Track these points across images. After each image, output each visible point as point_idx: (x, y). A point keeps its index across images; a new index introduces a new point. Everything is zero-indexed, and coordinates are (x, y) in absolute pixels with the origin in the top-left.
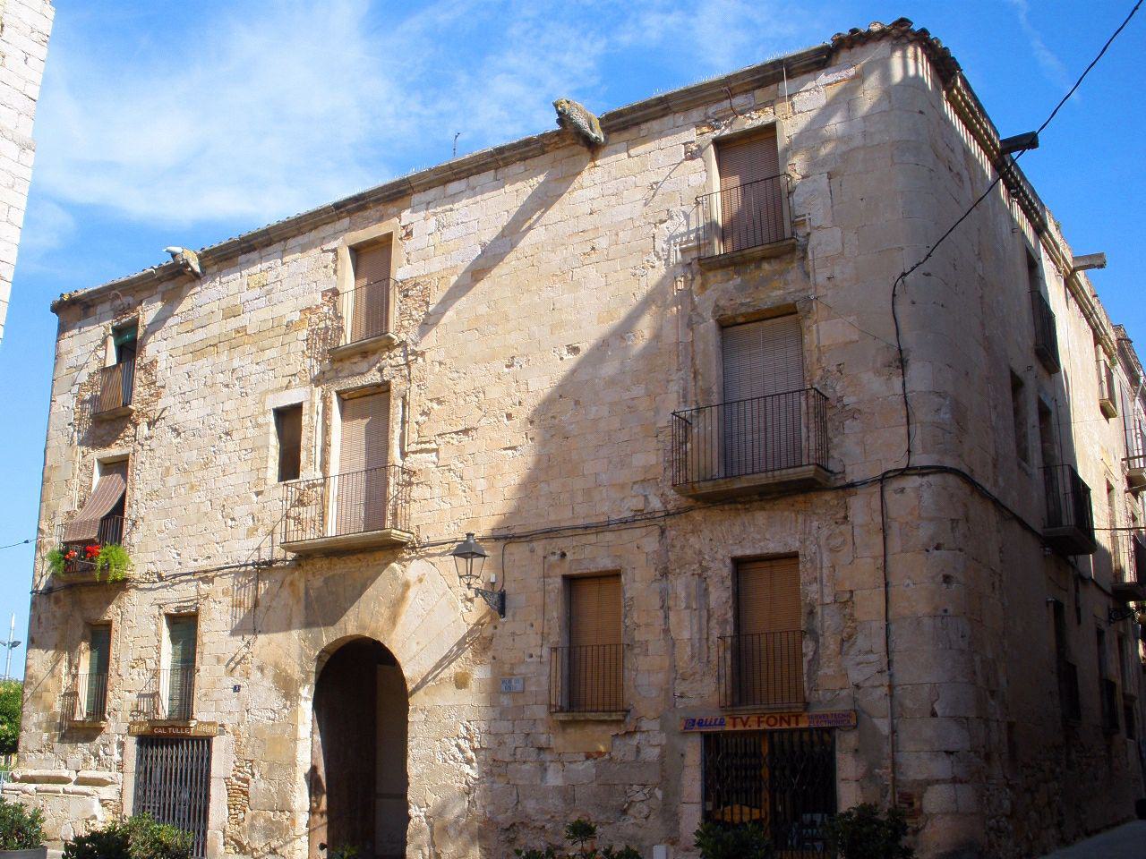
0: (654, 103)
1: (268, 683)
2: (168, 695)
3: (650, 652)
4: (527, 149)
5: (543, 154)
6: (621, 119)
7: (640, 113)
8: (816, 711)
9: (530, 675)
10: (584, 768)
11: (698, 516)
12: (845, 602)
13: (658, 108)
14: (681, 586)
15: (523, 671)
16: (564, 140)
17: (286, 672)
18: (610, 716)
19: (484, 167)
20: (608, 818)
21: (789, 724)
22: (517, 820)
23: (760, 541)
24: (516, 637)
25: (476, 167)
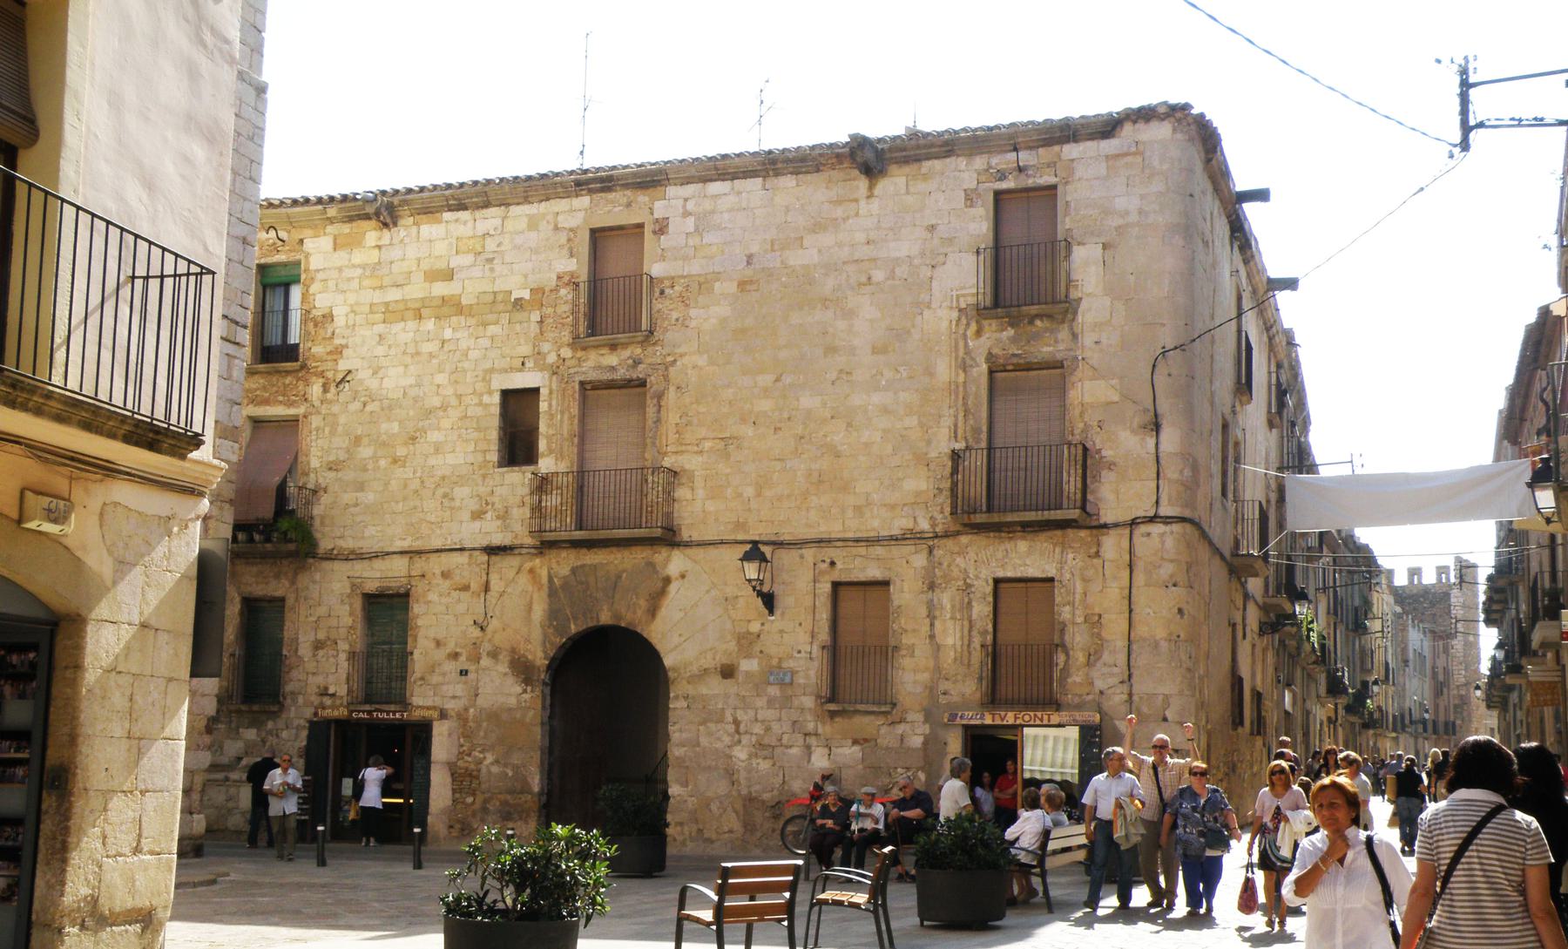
1: (503, 667)
11: (964, 539)
14: (946, 599)
22: (784, 798)
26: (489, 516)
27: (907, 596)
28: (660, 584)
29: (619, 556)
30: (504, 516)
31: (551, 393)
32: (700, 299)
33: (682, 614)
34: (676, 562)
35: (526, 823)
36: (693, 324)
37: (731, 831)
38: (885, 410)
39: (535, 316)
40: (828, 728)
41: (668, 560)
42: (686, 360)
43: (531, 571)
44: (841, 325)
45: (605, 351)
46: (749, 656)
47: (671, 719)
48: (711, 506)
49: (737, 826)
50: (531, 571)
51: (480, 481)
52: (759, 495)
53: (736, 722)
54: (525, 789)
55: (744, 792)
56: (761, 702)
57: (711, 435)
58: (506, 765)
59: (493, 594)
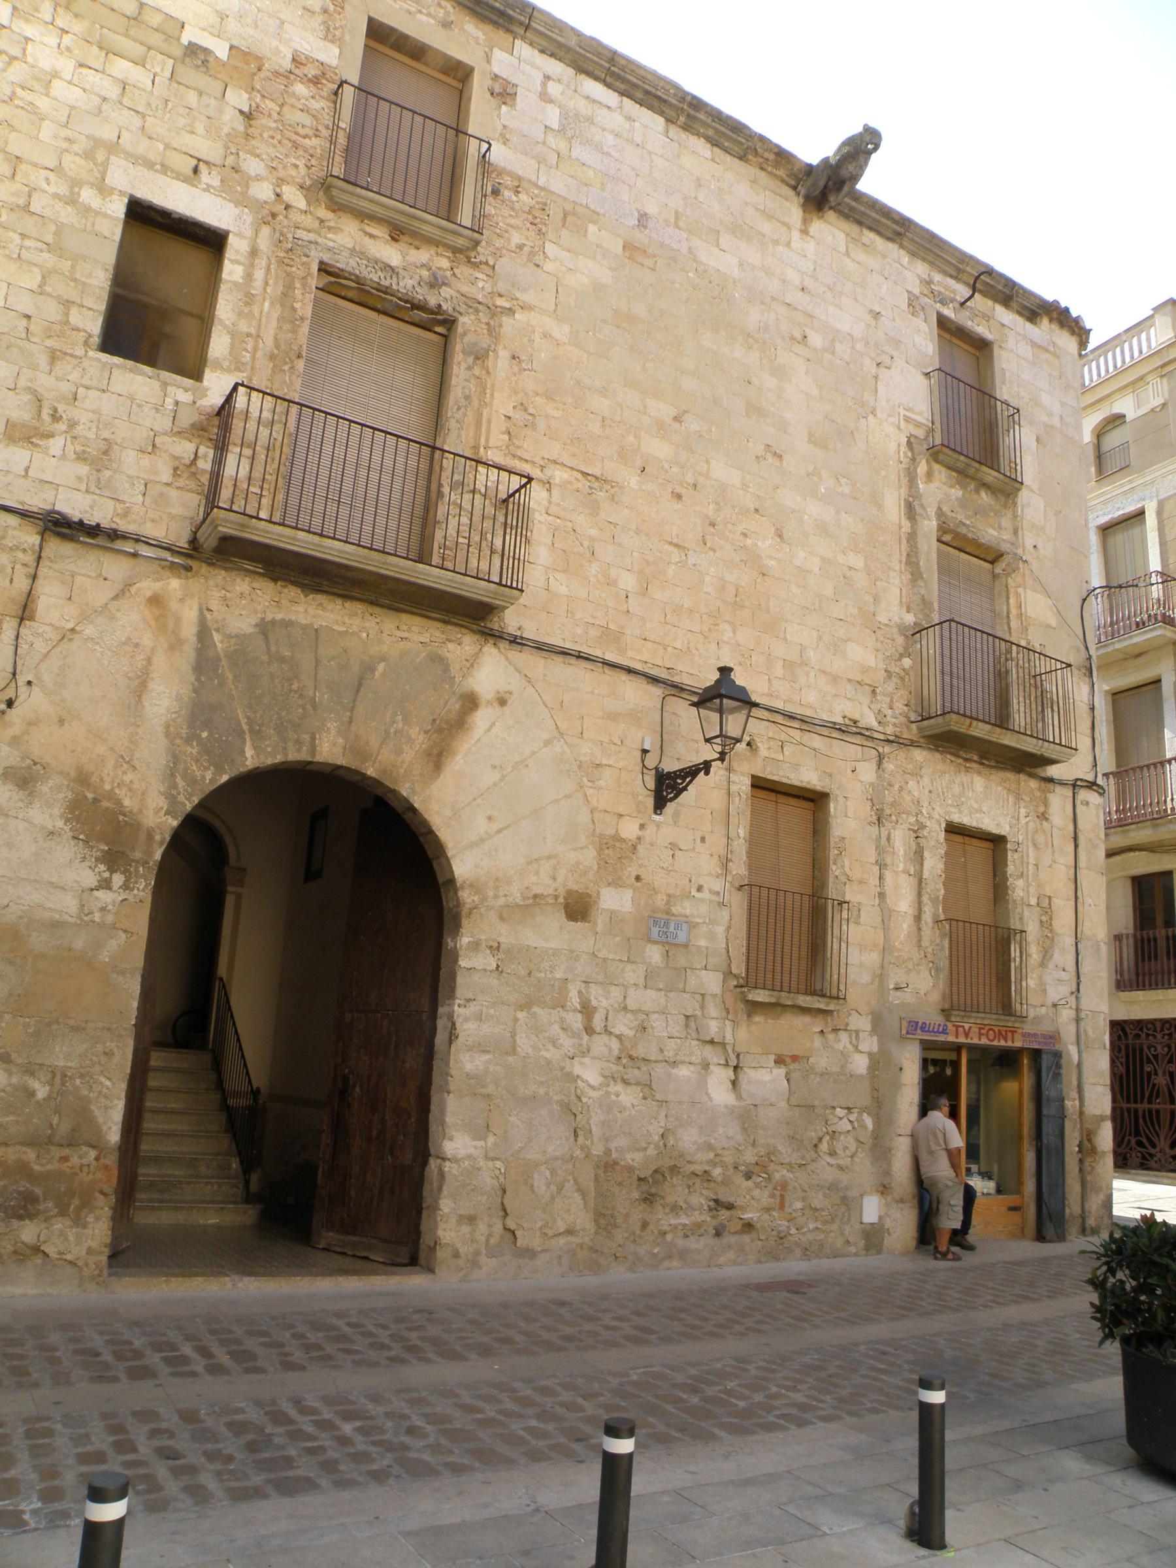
0: (897, 218)
1: (47, 814)
3: (862, 921)
4: (730, 133)
5: (740, 158)
6: (854, 203)
7: (874, 215)
8: (1029, 1028)
9: (698, 920)
10: (766, 1079)
11: (919, 755)
12: (1046, 908)
13: (896, 227)
14: (900, 839)
15: (688, 912)
16: (777, 165)
17: (119, 802)
18: (828, 1004)
19: (656, 103)
20: (803, 1158)
21: (1006, 1040)
22: (667, 1162)
23: (977, 811)
24: (678, 853)
25: (647, 93)
26: (56, 445)
27: (852, 823)
28: (455, 706)
29: (371, 624)
30: (99, 458)
31: (254, 253)
32: (565, 233)
33: (496, 776)
34: (491, 671)
35: (78, 1222)
36: (549, 266)
37: (570, 1232)
38: (823, 529)
39: (238, 99)
40: (742, 1033)
41: (472, 663)
42: (533, 318)
43: (156, 601)
44: (770, 382)
45: (381, 232)
46: (616, 883)
47: (461, 991)
48: (561, 585)
49: (583, 1220)
50: (156, 601)
51: (43, 361)
52: (644, 591)
53: (587, 1010)
54: (82, 1132)
55: (597, 1150)
56: (633, 974)
57: (572, 462)
58: (30, 1070)
59: (38, 635)
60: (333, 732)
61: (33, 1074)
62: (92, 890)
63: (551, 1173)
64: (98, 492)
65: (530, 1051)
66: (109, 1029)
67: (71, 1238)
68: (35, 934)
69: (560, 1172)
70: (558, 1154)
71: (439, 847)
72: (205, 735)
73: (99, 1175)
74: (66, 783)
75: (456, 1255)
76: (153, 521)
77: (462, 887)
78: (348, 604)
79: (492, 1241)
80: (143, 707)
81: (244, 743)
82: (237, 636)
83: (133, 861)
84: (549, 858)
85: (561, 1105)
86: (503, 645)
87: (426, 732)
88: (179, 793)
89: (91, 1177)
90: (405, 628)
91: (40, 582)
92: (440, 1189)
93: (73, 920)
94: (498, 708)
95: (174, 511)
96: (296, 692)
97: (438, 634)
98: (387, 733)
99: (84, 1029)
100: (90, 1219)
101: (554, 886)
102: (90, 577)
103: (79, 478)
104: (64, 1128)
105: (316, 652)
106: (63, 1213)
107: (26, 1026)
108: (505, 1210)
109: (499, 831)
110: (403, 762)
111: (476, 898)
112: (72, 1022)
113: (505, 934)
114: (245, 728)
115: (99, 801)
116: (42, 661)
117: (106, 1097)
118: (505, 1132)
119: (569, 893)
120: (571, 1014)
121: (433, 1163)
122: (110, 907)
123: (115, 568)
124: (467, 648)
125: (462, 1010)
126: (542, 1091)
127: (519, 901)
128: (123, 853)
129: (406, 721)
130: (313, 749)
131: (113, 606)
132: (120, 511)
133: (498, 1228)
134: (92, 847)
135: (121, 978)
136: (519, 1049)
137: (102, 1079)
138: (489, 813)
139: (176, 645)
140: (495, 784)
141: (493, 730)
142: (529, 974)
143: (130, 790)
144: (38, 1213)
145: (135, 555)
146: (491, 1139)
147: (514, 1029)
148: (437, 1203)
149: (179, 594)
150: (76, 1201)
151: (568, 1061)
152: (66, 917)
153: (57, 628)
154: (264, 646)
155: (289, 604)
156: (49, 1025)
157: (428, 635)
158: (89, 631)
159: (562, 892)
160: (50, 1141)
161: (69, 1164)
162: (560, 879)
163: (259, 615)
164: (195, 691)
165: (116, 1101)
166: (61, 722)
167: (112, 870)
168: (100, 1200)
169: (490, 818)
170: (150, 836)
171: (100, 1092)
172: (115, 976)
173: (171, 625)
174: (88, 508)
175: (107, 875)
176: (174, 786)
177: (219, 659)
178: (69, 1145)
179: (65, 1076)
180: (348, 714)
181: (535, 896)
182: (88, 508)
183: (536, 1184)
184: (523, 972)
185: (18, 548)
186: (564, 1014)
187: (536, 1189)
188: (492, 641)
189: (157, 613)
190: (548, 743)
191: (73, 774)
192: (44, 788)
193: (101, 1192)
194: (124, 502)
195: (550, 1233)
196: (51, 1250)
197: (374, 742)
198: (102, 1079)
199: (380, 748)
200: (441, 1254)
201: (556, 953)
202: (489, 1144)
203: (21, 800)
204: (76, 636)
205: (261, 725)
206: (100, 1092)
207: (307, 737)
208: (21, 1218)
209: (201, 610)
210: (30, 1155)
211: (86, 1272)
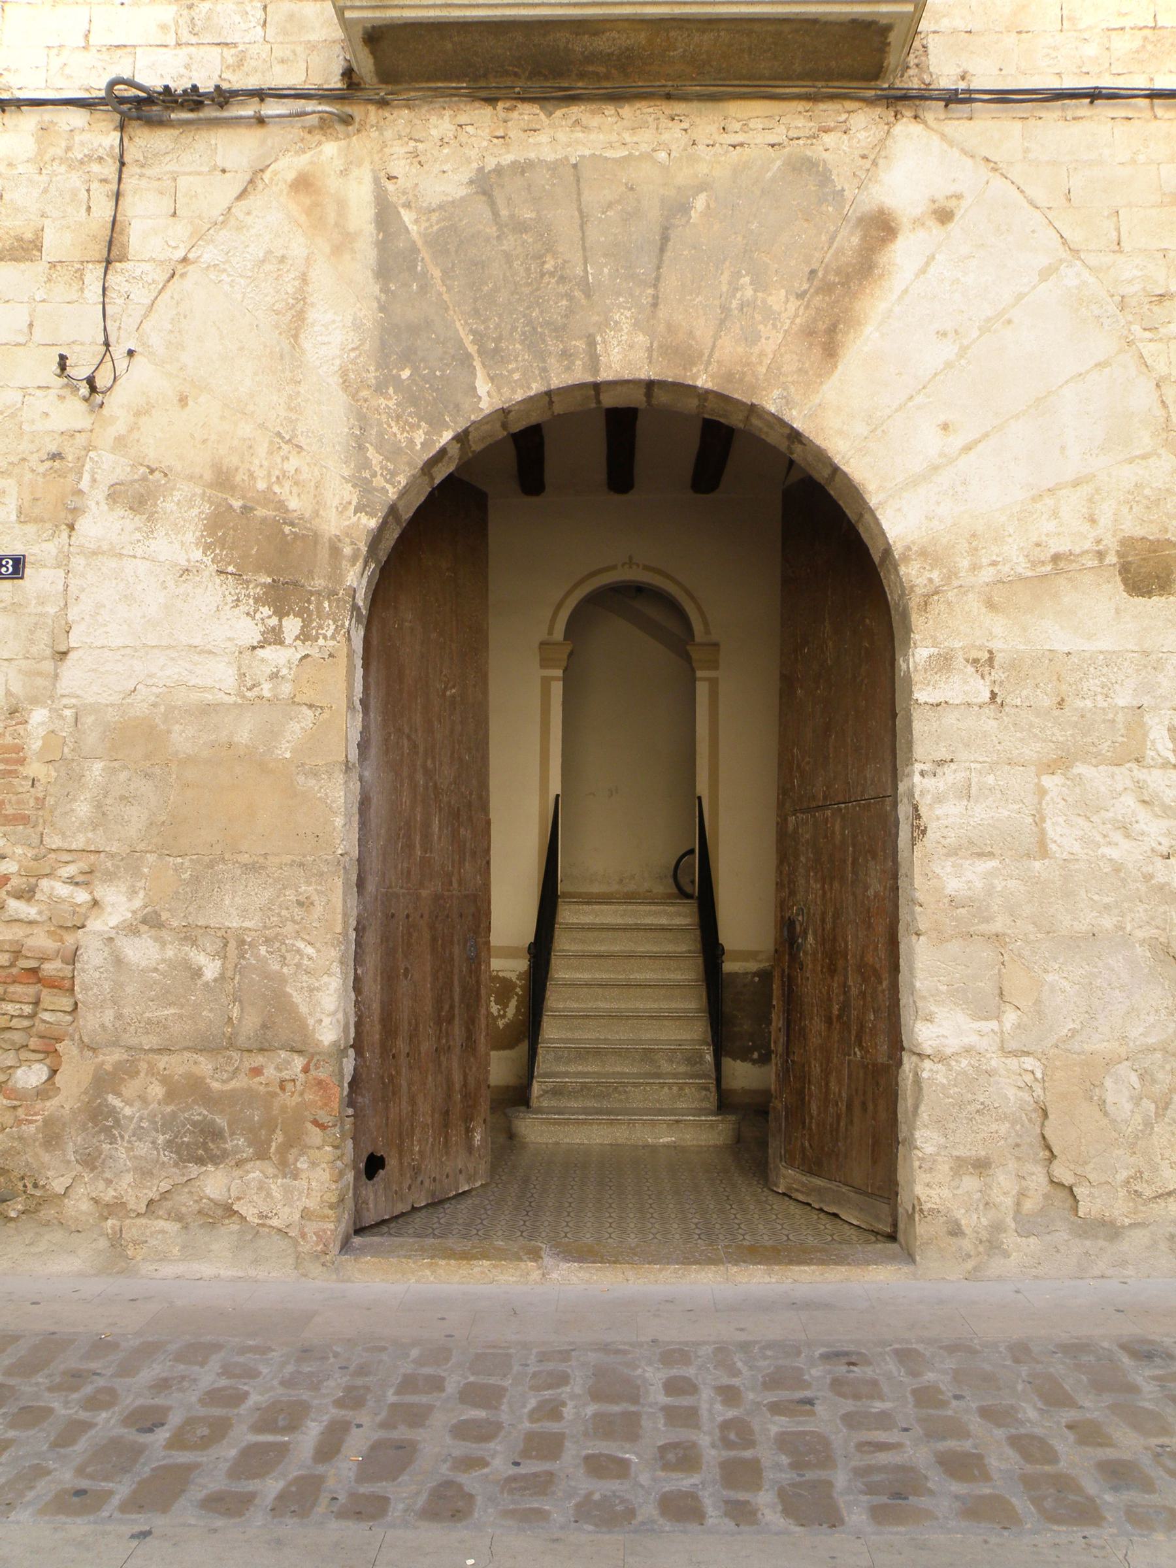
1: (178, 541)
2: (216, 110)
17: (281, 506)
29: (674, 134)
33: (948, 350)
34: (907, 163)
35: (286, 1168)
43: (303, 184)
59: (134, 280)
60: (626, 327)
61: (194, 943)
62: (254, 648)
63: (1141, 1077)
64: (194, 40)
65: (1077, 848)
66: (301, 865)
67: (277, 1194)
68: (177, 728)
69: (1160, 1076)
70: (1151, 1040)
71: (854, 492)
72: (406, 374)
73: (309, 1096)
74: (199, 491)
75: (956, 1231)
76: (283, 61)
77: (906, 558)
78: (627, 110)
79: (1028, 1205)
80: (303, 351)
81: (473, 374)
82: (441, 207)
83: (312, 593)
84: (1076, 483)
85: (1152, 948)
86: (933, 112)
87: (800, 296)
88: (374, 475)
89: (296, 1099)
90: (737, 126)
91: (126, 202)
92: (916, 1107)
93: (231, 699)
94: (936, 229)
95: (313, 37)
96: (552, 274)
97: (800, 122)
98: (725, 309)
99: (263, 868)
100: (302, 1164)
101: (1093, 534)
102: (199, 174)
103: (164, 27)
104: (250, 1023)
105: (579, 200)
106: (262, 1155)
107: (178, 869)
108: (1048, 1148)
109: (967, 448)
110: (762, 354)
111: (935, 575)
112: (245, 858)
113: (1001, 633)
114: (472, 349)
115: (252, 509)
116: (146, 316)
117: (307, 973)
118: (1038, 1002)
119: (1128, 544)
120: (1157, 773)
121: (908, 1062)
122: (284, 672)
123: (233, 148)
124: (862, 135)
125: (929, 783)
126: (1108, 922)
127: (1023, 569)
128: (295, 584)
129: (759, 284)
130: (594, 360)
131: (239, 210)
132: (230, 61)
133: (1038, 1181)
134: (248, 582)
135: (312, 782)
136: (1053, 847)
137: (301, 945)
138: (942, 418)
139: (343, 244)
140: (949, 365)
141: (932, 270)
142: (1061, 704)
143: (296, 483)
144: (225, 1154)
145: (261, 121)
146: (1011, 1017)
147: (1040, 811)
148: (912, 1135)
149: (339, 164)
150: (279, 1137)
151: (1159, 863)
152: (222, 694)
153: (162, 262)
154: (488, 214)
155: (521, 134)
156: (211, 865)
157: (782, 129)
158: (208, 254)
159: (1111, 543)
160: (231, 1045)
161: (261, 1079)
162: (1105, 520)
163: (475, 165)
164: (382, 308)
165: (325, 979)
166: (183, 401)
167: (281, 613)
168: (315, 1136)
169: (945, 427)
170: (335, 551)
171: (298, 966)
172: (301, 779)
173: (331, 218)
174: (183, 71)
175: (274, 621)
176: (366, 464)
177: (414, 249)
178: (262, 1050)
179: (243, 942)
180: (650, 291)
181: (1056, 558)
182: (183, 71)
183: (1110, 1099)
184: (1047, 702)
185: (90, 157)
186: (1140, 774)
187: (1110, 1108)
188: (909, 113)
189: (308, 202)
190: (1046, 274)
191: (208, 476)
192: (168, 505)
193: (316, 1123)
194: (235, 45)
195: (1148, 1192)
196: (248, 1211)
197: (703, 329)
198: (301, 945)
199: (716, 337)
200: (922, 1229)
201: (1111, 659)
202: (1008, 1026)
203: (138, 529)
204: (190, 268)
205: (499, 339)
206: (298, 966)
207: (580, 344)
208: (200, 1161)
209: (376, 180)
210: (204, 1066)
211: (305, 1247)
